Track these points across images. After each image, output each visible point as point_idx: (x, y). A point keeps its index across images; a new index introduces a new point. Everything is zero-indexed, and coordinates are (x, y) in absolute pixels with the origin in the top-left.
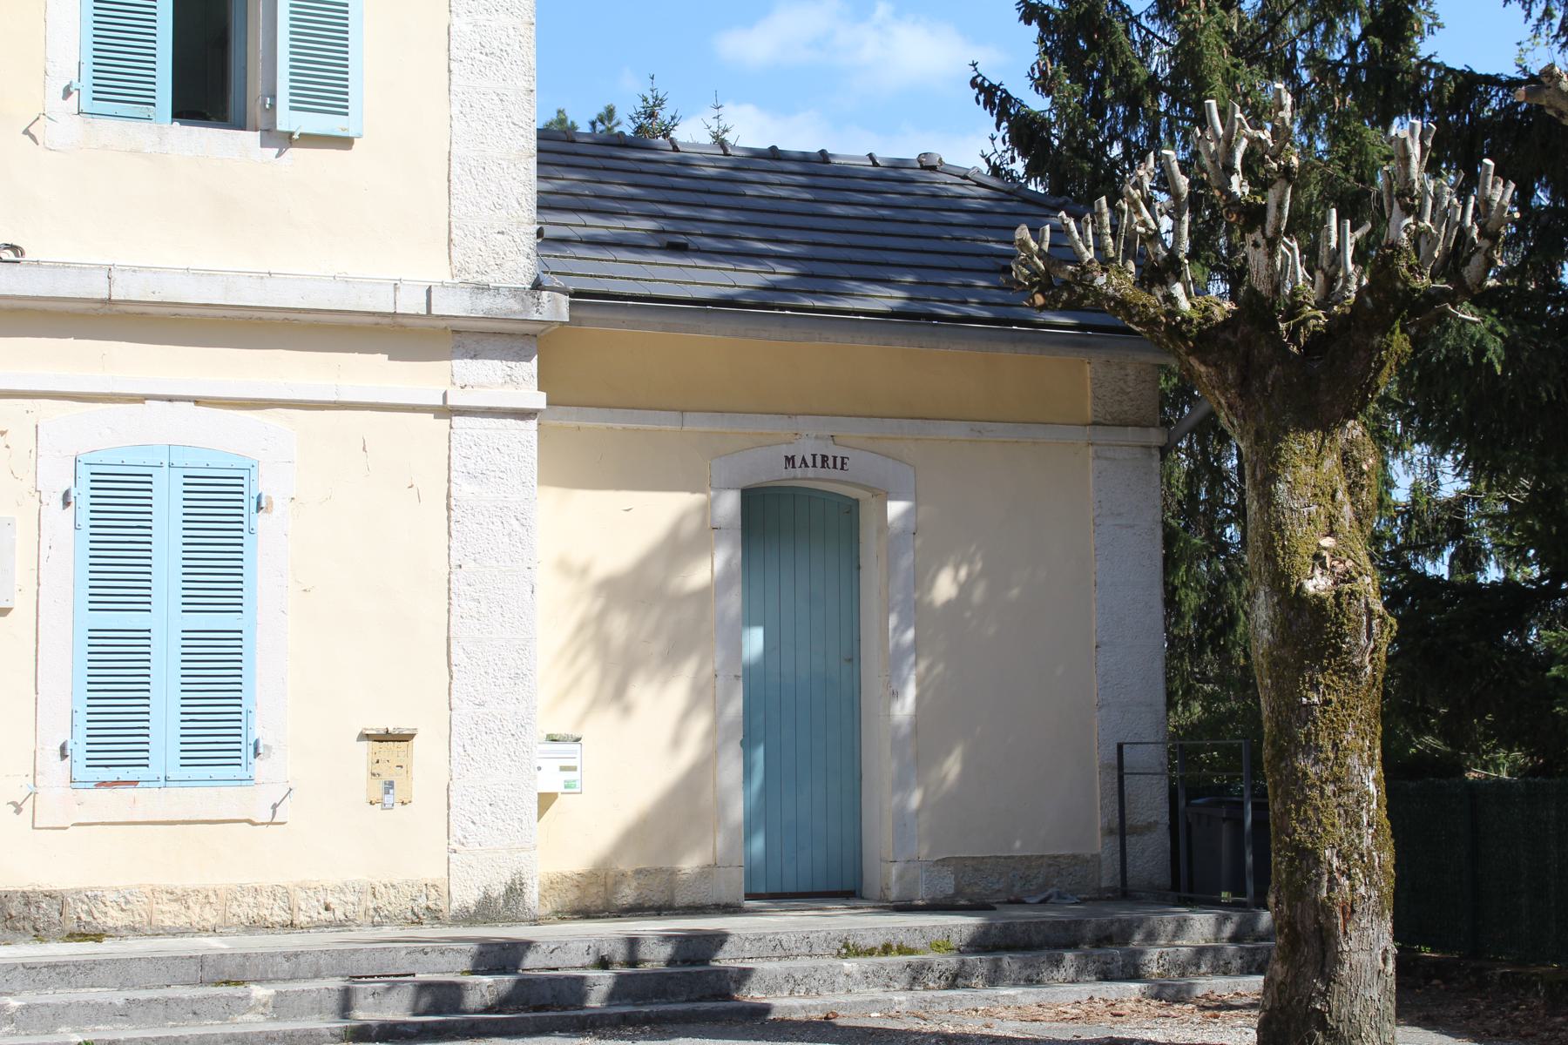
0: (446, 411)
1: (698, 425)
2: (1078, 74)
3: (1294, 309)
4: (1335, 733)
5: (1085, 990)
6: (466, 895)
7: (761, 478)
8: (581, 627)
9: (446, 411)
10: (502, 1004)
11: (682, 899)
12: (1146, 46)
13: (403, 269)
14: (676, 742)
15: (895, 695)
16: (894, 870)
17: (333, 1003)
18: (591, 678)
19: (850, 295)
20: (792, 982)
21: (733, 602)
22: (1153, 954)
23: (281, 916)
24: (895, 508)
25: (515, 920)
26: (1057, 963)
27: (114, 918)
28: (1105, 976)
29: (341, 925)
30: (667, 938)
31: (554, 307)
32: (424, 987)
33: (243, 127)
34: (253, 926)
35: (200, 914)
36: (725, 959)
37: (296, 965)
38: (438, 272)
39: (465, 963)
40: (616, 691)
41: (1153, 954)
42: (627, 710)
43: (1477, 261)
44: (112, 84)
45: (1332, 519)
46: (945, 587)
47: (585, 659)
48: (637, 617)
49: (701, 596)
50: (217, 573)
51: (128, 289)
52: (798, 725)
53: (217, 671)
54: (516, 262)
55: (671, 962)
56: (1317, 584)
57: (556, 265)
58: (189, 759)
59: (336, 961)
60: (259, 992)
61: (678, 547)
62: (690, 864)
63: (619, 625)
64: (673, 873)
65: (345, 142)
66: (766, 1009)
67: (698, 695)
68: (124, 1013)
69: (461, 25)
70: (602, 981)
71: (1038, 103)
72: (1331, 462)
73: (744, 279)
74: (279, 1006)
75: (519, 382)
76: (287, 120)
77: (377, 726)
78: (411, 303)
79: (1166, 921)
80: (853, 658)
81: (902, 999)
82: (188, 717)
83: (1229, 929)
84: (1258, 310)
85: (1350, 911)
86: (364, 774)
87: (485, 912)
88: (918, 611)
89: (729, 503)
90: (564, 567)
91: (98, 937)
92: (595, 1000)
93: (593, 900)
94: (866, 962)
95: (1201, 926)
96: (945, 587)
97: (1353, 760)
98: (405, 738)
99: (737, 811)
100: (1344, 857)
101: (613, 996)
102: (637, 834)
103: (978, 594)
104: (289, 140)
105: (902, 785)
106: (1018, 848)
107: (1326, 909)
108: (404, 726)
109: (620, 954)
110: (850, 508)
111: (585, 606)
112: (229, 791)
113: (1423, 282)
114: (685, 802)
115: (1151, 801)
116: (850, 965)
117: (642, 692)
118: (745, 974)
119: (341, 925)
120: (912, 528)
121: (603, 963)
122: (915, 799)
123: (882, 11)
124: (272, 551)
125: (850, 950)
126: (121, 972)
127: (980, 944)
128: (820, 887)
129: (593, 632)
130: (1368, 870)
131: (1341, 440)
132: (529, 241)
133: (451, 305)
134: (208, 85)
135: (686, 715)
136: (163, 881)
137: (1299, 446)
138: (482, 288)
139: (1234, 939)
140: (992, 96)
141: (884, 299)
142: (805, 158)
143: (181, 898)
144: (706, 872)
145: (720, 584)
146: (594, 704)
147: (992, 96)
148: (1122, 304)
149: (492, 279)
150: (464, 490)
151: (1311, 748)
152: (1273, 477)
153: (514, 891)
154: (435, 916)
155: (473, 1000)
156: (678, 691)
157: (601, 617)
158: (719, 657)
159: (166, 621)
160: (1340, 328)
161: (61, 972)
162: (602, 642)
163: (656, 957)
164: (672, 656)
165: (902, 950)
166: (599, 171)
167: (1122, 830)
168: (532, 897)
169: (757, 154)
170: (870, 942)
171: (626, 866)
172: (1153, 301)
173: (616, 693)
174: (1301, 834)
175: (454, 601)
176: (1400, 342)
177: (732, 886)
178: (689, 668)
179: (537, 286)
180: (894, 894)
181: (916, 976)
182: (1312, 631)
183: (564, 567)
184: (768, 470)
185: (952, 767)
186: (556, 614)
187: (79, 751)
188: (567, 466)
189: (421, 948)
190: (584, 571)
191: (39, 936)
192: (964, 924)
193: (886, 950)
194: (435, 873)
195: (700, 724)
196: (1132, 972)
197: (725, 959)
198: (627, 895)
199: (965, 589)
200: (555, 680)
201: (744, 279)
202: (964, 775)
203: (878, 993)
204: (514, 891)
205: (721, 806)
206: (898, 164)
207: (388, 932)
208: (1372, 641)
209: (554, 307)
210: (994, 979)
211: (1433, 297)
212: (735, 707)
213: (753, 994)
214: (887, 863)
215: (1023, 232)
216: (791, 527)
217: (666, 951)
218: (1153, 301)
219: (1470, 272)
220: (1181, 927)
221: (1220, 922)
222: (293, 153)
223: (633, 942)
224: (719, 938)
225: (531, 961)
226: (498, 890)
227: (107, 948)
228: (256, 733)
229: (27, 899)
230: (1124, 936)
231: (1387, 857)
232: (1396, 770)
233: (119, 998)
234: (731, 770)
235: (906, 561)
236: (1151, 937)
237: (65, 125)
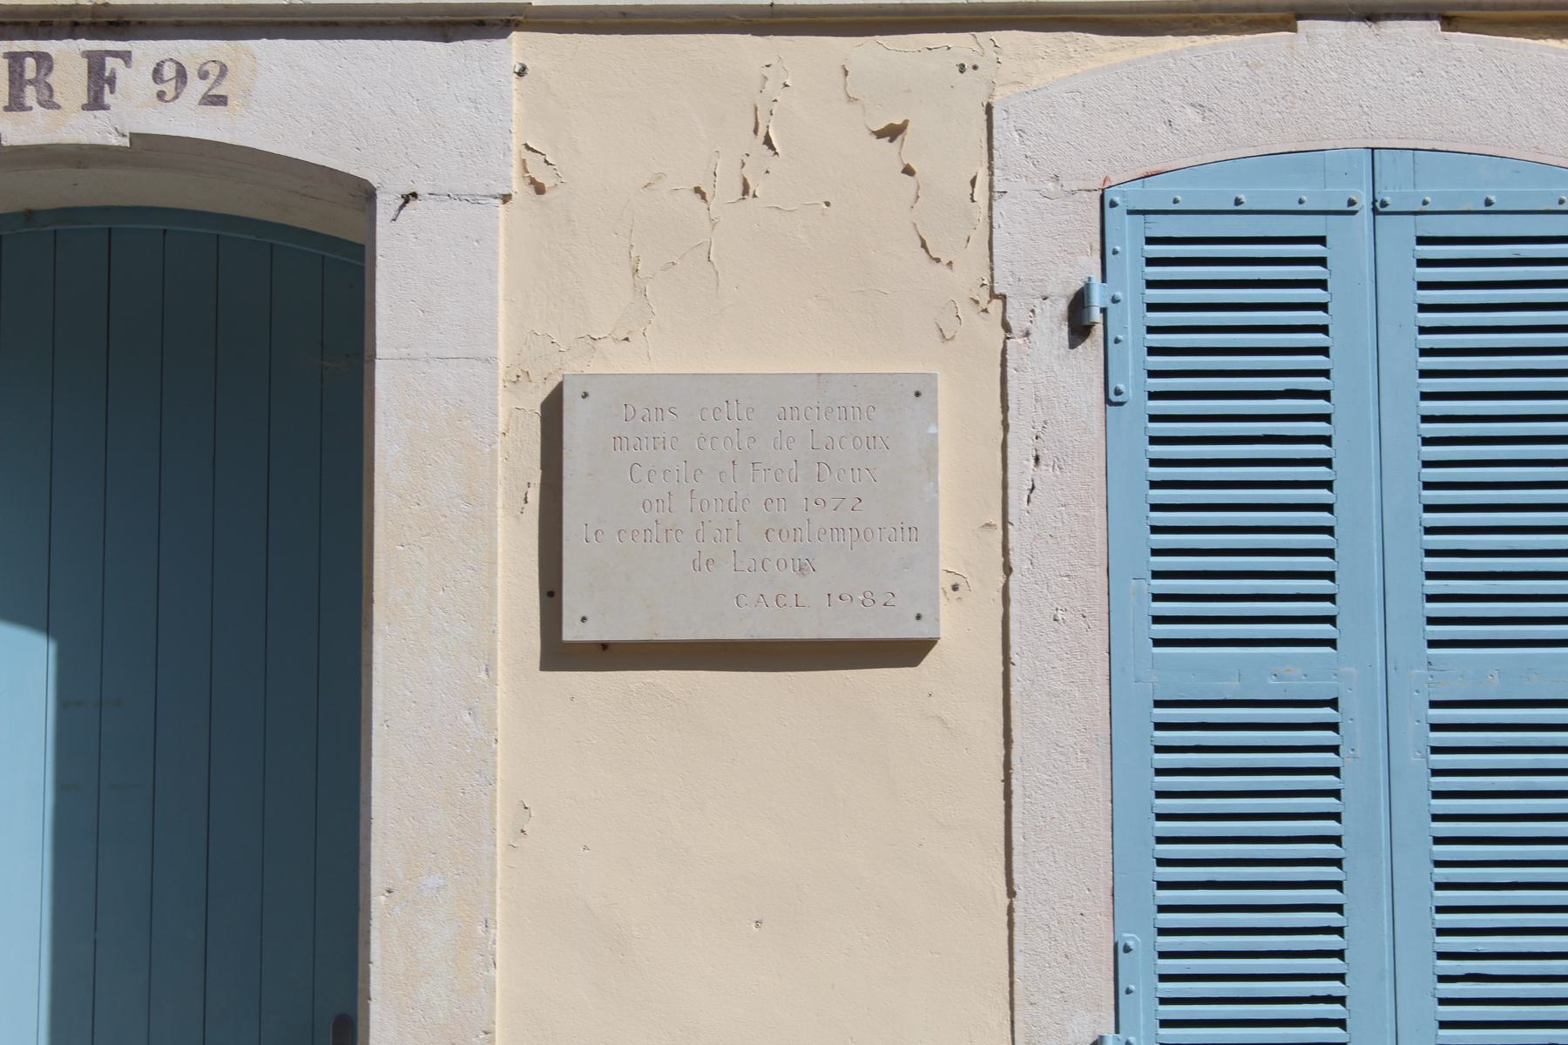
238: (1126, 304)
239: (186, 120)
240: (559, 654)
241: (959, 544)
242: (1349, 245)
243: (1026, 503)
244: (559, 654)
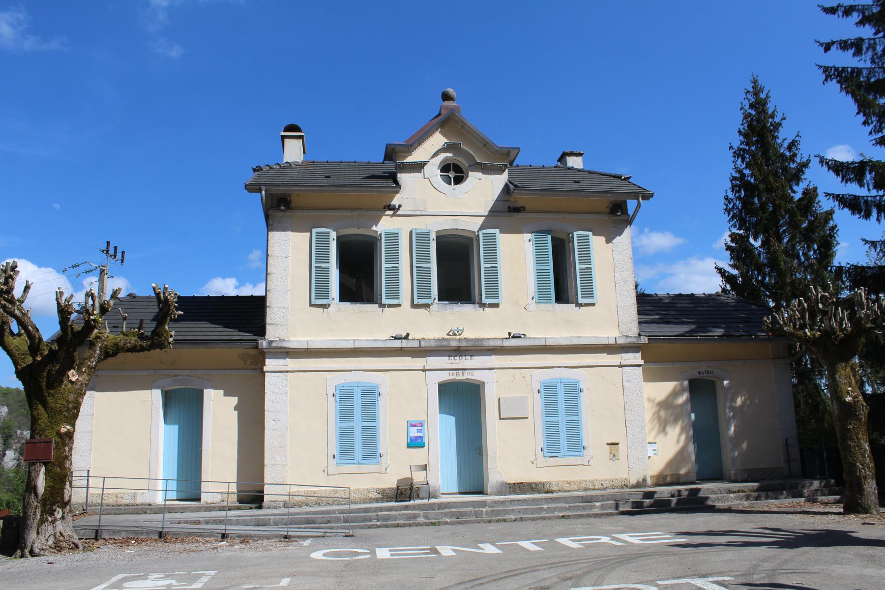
0: (621, 366)
1: (677, 365)
2: (744, 264)
3: (835, 333)
4: (857, 435)
5: (790, 500)
6: (633, 481)
7: (693, 377)
8: (654, 414)
9: (621, 366)
10: (651, 506)
11: (682, 481)
12: (759, 255)
13: (609, 334)
14: (678, 441)
15: (729, 429)
16: (733, 472)
17: (614, 506)
18: (657, 427)
19: (710, 331)
20: (718, 499)
21: (689, 407)
22: (806, 491)
23: (592, 487)
24: (725, 382)
25: (645, 487)
26: (782, 494)
27: (555, 488)
28: (794, 497)
29: (605, 489)
30: (686, 490)
31: (644, 340)
32: (634, 502)
33: (568, 303)
34: (586, 489)
35: (573, 487)
36: (701, 495)
37: (603, 498)
38: (617, 334)
39: (641, 497)
40: (663, 430)
41: (806, 491)
42: (666, 434)
43: (880, 319)
44: (542, 296)
45: (850, 383)
46: (739, 401)
47: (655, 422)
48: (667, 411)
49: (681, 405)
50: (573, 407)
51: (550, 343)
52: (705, 436)
53: (574, 429)
54: (633, 328)
55: (688, 495)
56: (848, 399)
57: (644, 329)
58: (569, 451)
59: (612, 497)
60: (598, 504)
61: (675, 394)
62: (683, 472)
63: (662, 413)
64: (679, 475)
65: (593, 305)
66: (714, 506)
67: (683, 430)
68: (569, 509)
69: (617, 275)
70: (674, 500)
71: (735, 272)
72: (848, 369)
73: (684, 329)
74: (602, 507)
75: (636, 358)
76: (581, 301)
77: (611, 441)
78: (612, 341)
79: (807, 482)
80: (716, 420)
81: (746, 503)
82: (568, 441)
83: (823, 484)
84: (828, 334)
85: (865, 478)
86: (608, 453)
87: (638, 485)
88: (732, 408)
89: (686, 383)
90: (649, 400)
91: (552, 492)
92: (673, 505)
93: (661, 480)
94: (736, 495)
95: (816, 484)
96: (739, 401)
97: (862, 441)
98: (617, 444)
99: (693, 458)
100: (862, 465)
101: (677, 504)
102: (670, 464)
103: (748, 402)
104: (581, 305)
105: (733, 450)
106: (761, 466)
107: (859, 478)
108: (617, 441)
109: (676, 494)
110: (713, 384)
111: (655, 409)
112: (579, 458)
113: (869, 325)
114: (679, 458)
115: (795, 453)
116: (731, 495)
117: (669, 429)
118: (707, 498)
119: (605, 489)
120: (730, 387)
121: (673, 496)
122: (736, 454)
123: (646, 230)
124: (585, 400)
125: (730, 492)
126: (565, 500)
127: (758, 490)
128: (193, 497)
129: (657, 415)
130: (869, 468)
131: (850, 363)
132: (635, 324)
133: (621, 341)
134: (562, 295)
135: (680, 434)
136: (565, 479)
137: (841, 366)
138: (627, 337)
139: (825, 487)
140: (722, 272)
141: (719, 332)
142: (688, 295)
143: (569, 483)
144: (687, 474)
145: (685, 403)
146: (658, 432)
147: (722, 272)
148: (791, 334)
149: (629, 334)
150: (626, 384)
151: (851, 439)
152: (835, 374)
153: (644, 480)
154: (626, 486)
155: (645, 505)
156: (678, 429)
157: (658, 412)
158: (686, 421)
159: (562, 418)
160: (848, 337)
161: (546, 500)
162: (659, 418)
163: (685, 494)
164: (676, 421)
165: (743, 491)
166: (647, 304)
167: (788, 460)
168: (649, 481)
169: (677, 295)
170: (735, 490)
171: (667, 472)
172: (800, 333)
173: (663, 430)
174: (851, 460)
175: (628, 412)
176: (863, 340)
177: (693, 477)
178: (680, 424)
179: (640, 335)
180: (733, 478)
181: (748, 498)
182: (849, 410)
183: (649, 400)
184: (694, 375)
185: (744, 446)
186: (649, 411)
187: (545, 449)
188: (649, 377)
189: (631, 494)
190: (654, 400)
191: (539, 492)
192: (755, 485)
193: (739, 491)
194: (625, 476)
195: (683, 437)
196: (801, 496)
197: (701, 495)
198: (668, 480)
199: (743, 403)
200: (650, 430)
201: (684, 329)
202: (748, 447)
203: (739, 502)
204: (644, 480)
205: (689, 457)
206: (710, 295)
207: (616, 490)
208: (863, 412)
209: (644, 340)
210: (767, 498)
211: (871, 328)
212: (691, 432)
213: (710, 503)
214: (730, 468)
215: (765, 318)
216: (701, 390)
217: (687, 493)
218: (800, 333)
219: (879, 322)
220: (811, 484)
221: (821, 483)
222: (583, 308)
223: (679, 491)
224: (699, 490)
225: (656, 496)
226: (641, 480)
227: (554, 495)
228: (584, 444)
229: (536, 484)
230: (797, 487)
231: (872, 465)
232: (872, 443)
233: (567, 505)
234: (691, 448)
235: (729, 396)
236: (803, 487)
237: (533, 306)
238: (337, 396)
239: (470, 377)
240: (500, 419)
241: (530, 410)
242: (559, 385)
243: (535, 406)
244: (500, 419)
